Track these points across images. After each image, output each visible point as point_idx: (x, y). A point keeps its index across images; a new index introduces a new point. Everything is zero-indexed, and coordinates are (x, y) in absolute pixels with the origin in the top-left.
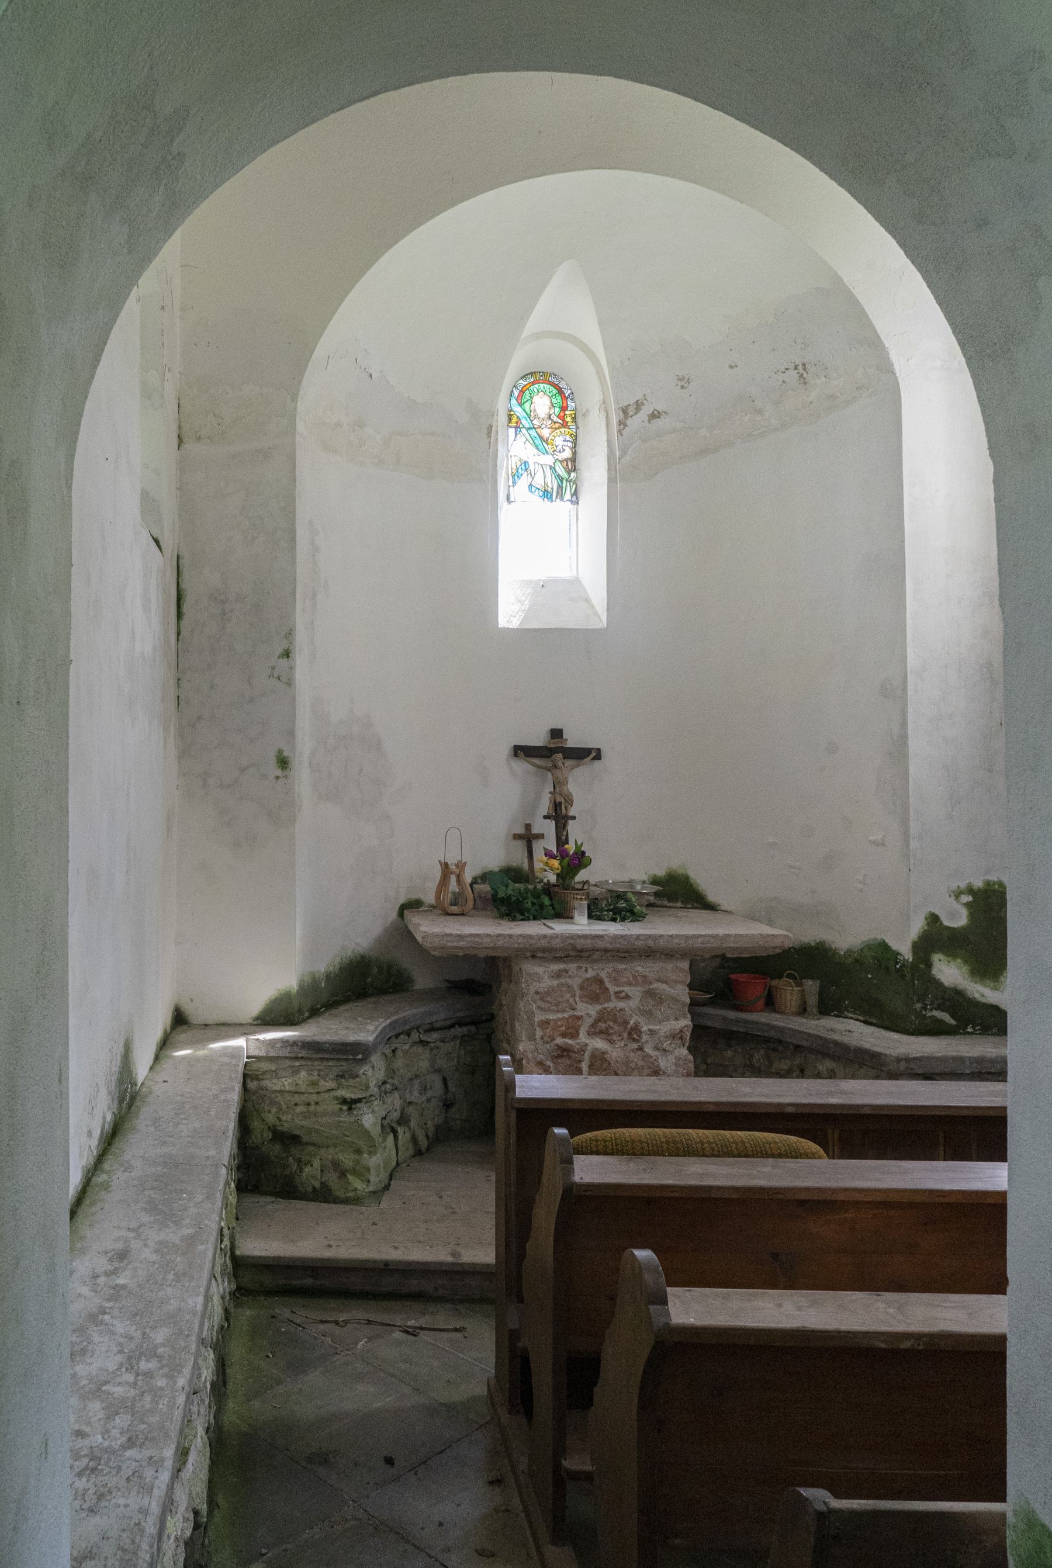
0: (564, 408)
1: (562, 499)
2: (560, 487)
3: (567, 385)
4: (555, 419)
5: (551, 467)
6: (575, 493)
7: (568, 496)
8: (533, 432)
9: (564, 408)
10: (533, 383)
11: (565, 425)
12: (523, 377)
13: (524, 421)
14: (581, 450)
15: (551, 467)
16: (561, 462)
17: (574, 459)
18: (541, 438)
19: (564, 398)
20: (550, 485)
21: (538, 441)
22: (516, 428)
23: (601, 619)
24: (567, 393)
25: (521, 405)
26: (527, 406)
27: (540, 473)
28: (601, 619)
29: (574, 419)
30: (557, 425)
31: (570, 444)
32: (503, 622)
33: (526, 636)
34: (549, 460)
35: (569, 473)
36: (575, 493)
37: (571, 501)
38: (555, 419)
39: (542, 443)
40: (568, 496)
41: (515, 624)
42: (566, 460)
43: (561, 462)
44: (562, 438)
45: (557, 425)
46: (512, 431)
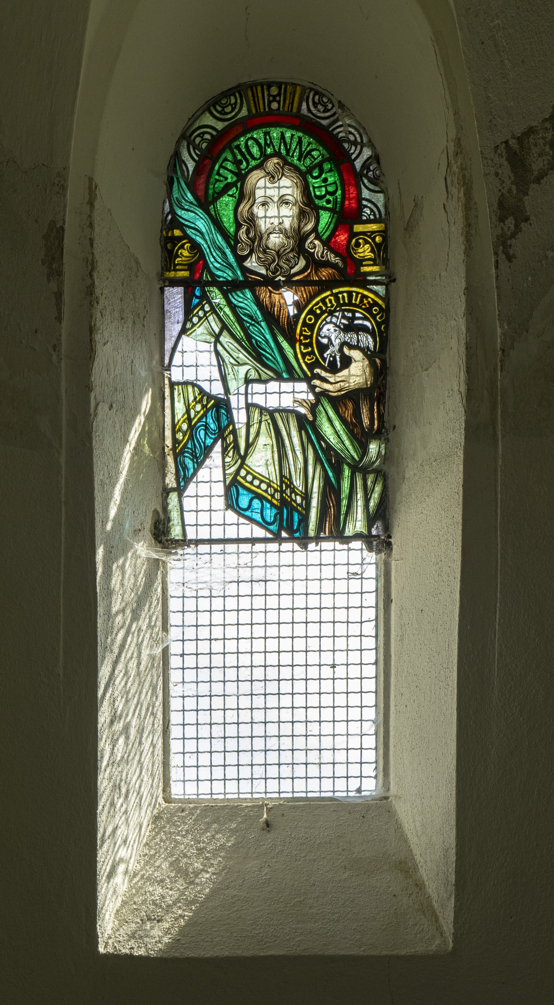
0: (347, 216)
1: (338, 535)
2: (330, 490)
3: (361, 128)
4: (317, 248)
5: (301, 420)
6: (382, 515)
7: (357, 523)
8: (245, 300)
9: (347, 216)
10: (248, 125)
11: (350, 273)
12: (213, 105)
13: (214, 262)
14: (400, 362)
15: (301, 420)
16: (337, 402)
17: (378, 391)
18: (271, 317)
19: (350, 177)
20: (298, 483)
21: (262, 332)
22: (188, 285)
23: (183, 288)
24: (361, 157)
25: (206, 203)
26: (226, 206)
27: (265, 440)
28: (183, 288)
29: (382, 252)
30: (325, 273)
31: (367, 341)
32: (112, 930)
33: (107, 956)
34: (289, 395)
35: (361, 438)
36: (382, 515)
37: (366, 538)
38: (317, 248)
39: (275, 344)
40: (357, 523)
41: (157, 939)
42: (354, 396)
43: (337, 402)
44: (339, 319)
45: (325, 273)
46: (175, 297)
